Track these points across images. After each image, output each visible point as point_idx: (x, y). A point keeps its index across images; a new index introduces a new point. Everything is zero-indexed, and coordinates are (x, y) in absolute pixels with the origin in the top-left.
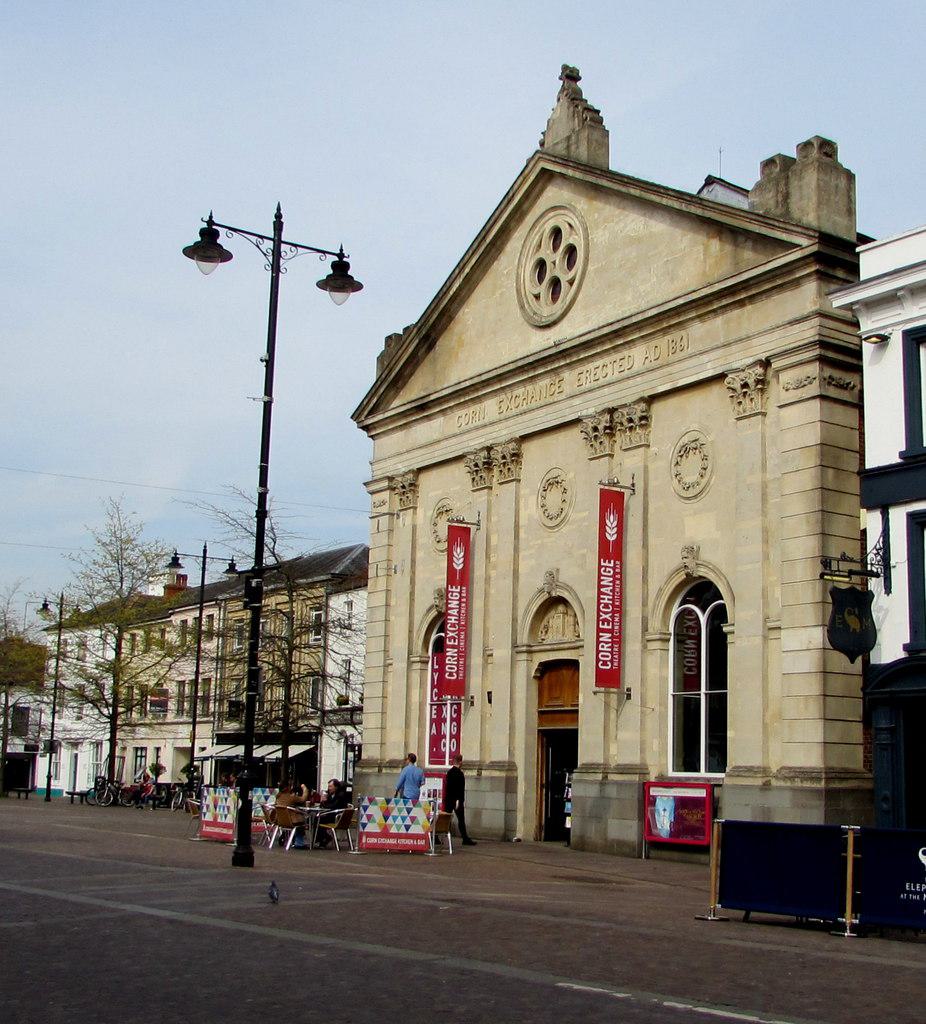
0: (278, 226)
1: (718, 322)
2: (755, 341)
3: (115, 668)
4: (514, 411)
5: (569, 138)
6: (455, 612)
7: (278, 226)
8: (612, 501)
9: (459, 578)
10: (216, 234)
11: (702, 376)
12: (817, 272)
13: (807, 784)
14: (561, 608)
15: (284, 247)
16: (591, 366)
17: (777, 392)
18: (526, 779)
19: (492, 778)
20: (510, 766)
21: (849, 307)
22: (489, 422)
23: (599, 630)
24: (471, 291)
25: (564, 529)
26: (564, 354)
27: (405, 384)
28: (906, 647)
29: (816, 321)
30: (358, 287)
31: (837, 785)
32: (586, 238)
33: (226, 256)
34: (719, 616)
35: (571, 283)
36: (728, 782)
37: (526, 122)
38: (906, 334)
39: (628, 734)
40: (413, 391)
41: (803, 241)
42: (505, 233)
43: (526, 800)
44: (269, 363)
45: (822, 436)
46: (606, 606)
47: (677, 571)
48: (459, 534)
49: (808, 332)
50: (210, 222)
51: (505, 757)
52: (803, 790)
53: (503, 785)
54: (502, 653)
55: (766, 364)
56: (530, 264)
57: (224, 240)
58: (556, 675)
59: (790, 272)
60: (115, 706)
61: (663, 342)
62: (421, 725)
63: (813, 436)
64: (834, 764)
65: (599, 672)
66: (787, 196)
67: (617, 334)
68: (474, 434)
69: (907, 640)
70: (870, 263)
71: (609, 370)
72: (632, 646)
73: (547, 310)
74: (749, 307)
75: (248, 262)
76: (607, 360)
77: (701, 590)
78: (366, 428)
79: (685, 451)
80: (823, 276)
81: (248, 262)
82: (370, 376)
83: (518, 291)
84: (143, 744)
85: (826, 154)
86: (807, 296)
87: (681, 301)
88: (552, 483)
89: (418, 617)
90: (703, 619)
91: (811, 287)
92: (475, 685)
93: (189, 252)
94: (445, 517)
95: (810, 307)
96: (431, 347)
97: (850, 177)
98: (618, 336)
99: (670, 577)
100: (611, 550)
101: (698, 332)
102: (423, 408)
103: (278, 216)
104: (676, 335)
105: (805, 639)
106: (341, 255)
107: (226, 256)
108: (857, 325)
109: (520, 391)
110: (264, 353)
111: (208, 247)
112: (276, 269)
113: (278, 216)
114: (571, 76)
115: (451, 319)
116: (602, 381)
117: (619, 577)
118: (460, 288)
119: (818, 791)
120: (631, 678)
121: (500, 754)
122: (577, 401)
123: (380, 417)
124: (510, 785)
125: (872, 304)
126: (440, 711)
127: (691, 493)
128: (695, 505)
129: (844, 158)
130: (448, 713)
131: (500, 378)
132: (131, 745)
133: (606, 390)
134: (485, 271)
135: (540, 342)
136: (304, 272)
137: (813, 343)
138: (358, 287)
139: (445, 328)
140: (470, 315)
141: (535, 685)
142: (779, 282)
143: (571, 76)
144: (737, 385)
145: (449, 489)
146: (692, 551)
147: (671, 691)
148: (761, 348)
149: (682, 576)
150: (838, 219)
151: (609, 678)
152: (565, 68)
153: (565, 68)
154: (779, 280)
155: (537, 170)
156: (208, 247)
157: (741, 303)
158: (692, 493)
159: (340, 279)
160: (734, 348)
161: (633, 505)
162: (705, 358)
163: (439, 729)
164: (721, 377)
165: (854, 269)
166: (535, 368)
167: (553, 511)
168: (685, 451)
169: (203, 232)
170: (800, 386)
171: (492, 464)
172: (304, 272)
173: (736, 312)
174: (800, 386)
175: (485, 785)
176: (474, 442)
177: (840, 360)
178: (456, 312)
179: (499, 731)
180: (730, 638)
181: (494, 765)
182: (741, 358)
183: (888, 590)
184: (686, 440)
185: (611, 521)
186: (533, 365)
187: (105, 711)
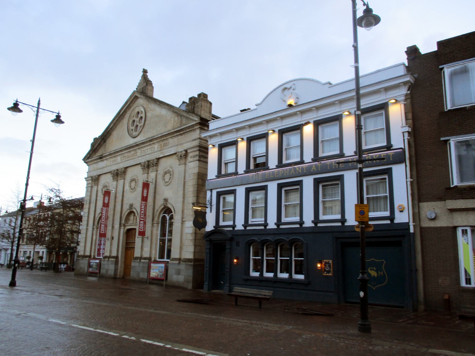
0: (39, 104)
1: (176, 139)
2: (184, 145)
3: (72, 228)
4: (125, 160)
5: (143, 88)
6: (104, 214)
7: (39, 104)
8: (146, 185)
9: (106, 205)
10: (18, 105)
11: (171, 153)
12: (200, 127)
13: (189, 263)
14: (133, 214)
15: (40, 110)
16: (144, 149)
17: (189, 159)
18: (121, 261)
19: (111, 261)
20: (117, 257)
21: (205, 137)
22: (118, 163)
23: (140, 220)
24: (116, 127)
25: (135, 193)
26: (137, 145)
27: (97, 151)
28: (214, 227)
29: (198, 140)
30: (62, 122)
31: (197, 263)
32: (146, 115)
33: (20, 111)
34: (171, 218)
35: (141, 126)
36: (170, 262)
37: (133, 84)
38: (219, 145)
39: (145, 248)
40: (99, 154)
41: (196, 119)
42: (125, 112)
43: (121, 266)
44: (33, 141)
45: (199, 171)
46: (143, 214)
47: (162, 205)
48: (107, 193)
49: (196, 143)
50: (17, 101)
51: (148, 256)
52: (188, 265)
53: (114, 263)
54: (117, 226)
55: (186, 151)
56: (131, 121)
57: (20, 107)
58: (130, 233)
59: (193, 127)
60: (13, 239)
61: (162, 143)
62: (95, 246)
63: (196, 170)
64: (196, 257)
65: (139, 231)
66: (194, 107)
67: (151, 141)
68: (114, 166)
69: (214, 225)
70: (213, 125)
71: (148, 150)
72: (149, 225)
73: (135, 134)
74: (183, 136)
75: (28, 113)
76: (148, 147)
77: (167, 210)
78: (86, 163)
79: (166, 173)
80: (201, 128)
81: (28, 113)
82: (88, 148)
83: (128, 128)
84: (38, 250)
85: (204, 97)
86: (196, 134)
87: (167, 133)
88: (132, 180)
89: (97, 215)
90: (168, 218)
91: (198, 131)
92: (109, 235)
93: (9, 109)
94: (105, 188)
95: (198, 137)
96: (105, 142)
97: (211, 104)
98: (151, 140)
99: (160, 207)
100: (144, 199)
101: (172, 141)
102: (101, 158)
103: (39, 101)
104: (165, 142)
105: (189, 225)
106: (58, 113)
107: (20, 111)
108: (207, 141)
109: (126, 155)
110: (32, 138)
111: (15, 108)
112: (37, 116)
113: (39, 101)
114: (145, 71)
115: (110, 134)
116: (147, 153)
117: (146, 206)
118: (113, 126)
119: (191, 265)
120: (148, 233)
121: (114, 254)
122: (140, 158)
123: (90, 160)
124: (116, 263)
125: (211, 137)
126: (101, 242)
127: (167, 184)
128: (168, 187)
129: (210, 99)
130: (102, 243)
131: (121, 151)
132: (22, 250)
133: (147, 156)
134: (120, 122)
135: (132, 141)
136: (46, 118)
137: (198, 146)
138: (62, 122)
139: (109, 137)
140: (115, 134)
141: (125, 235)
142: (190, 129)
143: (145, 71)
144: (179, 156)
145: (107, 180)
146: (166, 200)
147: (159, 237)
148: (186, 146)
149: (163, 207)
150: (207, 114)
151: (142, 234)
152: (144, 69)
153: (144, 69)
154: (190, 129)
155: (134, 96)
156: (15, 108)
157: (181, 134)
158: (167, 184)
159: (58, 120)
160: (179, 146)
161: (152, 187)
162: (172, 148)
163: (100, 247)
164: (175, 154)
165: (208, 126)
166: (173, 134)
167: (133, 187)
168: (166, 173)
169: (14, 104)
170: (194, 157)
171: (118, 174)
172: (46, 118)
173: (180, 137)
174: (194, 157)
175: (110, 263)
176: (114, 168)
177: (203, 151)
178: (112, 132)
179: (113, 248)
180: (174, 223)
181: (145, 259)
182: (181, 149)
183: (211, 211)
184: (166, 170)
185: (145, 191)
186: (130, 148)
187: (10, 240)
